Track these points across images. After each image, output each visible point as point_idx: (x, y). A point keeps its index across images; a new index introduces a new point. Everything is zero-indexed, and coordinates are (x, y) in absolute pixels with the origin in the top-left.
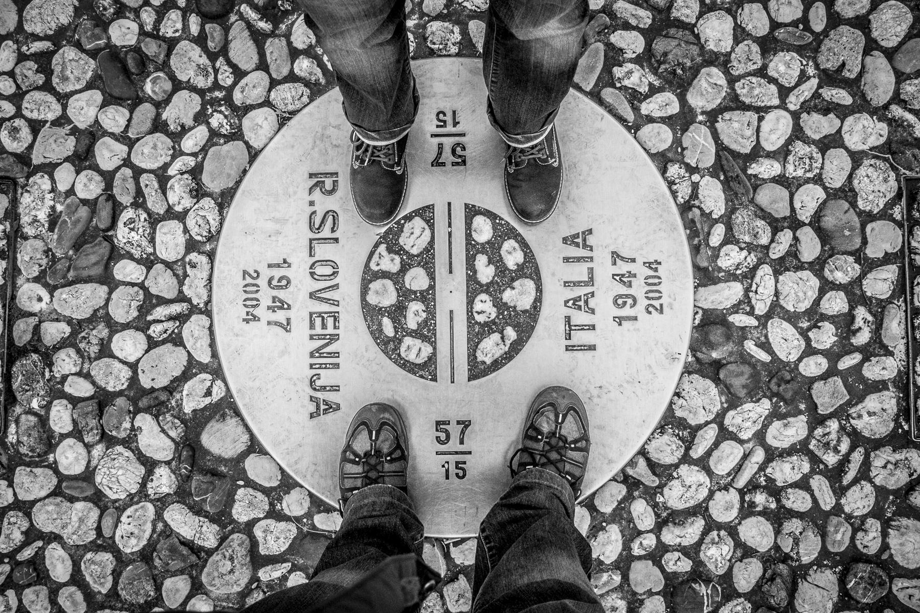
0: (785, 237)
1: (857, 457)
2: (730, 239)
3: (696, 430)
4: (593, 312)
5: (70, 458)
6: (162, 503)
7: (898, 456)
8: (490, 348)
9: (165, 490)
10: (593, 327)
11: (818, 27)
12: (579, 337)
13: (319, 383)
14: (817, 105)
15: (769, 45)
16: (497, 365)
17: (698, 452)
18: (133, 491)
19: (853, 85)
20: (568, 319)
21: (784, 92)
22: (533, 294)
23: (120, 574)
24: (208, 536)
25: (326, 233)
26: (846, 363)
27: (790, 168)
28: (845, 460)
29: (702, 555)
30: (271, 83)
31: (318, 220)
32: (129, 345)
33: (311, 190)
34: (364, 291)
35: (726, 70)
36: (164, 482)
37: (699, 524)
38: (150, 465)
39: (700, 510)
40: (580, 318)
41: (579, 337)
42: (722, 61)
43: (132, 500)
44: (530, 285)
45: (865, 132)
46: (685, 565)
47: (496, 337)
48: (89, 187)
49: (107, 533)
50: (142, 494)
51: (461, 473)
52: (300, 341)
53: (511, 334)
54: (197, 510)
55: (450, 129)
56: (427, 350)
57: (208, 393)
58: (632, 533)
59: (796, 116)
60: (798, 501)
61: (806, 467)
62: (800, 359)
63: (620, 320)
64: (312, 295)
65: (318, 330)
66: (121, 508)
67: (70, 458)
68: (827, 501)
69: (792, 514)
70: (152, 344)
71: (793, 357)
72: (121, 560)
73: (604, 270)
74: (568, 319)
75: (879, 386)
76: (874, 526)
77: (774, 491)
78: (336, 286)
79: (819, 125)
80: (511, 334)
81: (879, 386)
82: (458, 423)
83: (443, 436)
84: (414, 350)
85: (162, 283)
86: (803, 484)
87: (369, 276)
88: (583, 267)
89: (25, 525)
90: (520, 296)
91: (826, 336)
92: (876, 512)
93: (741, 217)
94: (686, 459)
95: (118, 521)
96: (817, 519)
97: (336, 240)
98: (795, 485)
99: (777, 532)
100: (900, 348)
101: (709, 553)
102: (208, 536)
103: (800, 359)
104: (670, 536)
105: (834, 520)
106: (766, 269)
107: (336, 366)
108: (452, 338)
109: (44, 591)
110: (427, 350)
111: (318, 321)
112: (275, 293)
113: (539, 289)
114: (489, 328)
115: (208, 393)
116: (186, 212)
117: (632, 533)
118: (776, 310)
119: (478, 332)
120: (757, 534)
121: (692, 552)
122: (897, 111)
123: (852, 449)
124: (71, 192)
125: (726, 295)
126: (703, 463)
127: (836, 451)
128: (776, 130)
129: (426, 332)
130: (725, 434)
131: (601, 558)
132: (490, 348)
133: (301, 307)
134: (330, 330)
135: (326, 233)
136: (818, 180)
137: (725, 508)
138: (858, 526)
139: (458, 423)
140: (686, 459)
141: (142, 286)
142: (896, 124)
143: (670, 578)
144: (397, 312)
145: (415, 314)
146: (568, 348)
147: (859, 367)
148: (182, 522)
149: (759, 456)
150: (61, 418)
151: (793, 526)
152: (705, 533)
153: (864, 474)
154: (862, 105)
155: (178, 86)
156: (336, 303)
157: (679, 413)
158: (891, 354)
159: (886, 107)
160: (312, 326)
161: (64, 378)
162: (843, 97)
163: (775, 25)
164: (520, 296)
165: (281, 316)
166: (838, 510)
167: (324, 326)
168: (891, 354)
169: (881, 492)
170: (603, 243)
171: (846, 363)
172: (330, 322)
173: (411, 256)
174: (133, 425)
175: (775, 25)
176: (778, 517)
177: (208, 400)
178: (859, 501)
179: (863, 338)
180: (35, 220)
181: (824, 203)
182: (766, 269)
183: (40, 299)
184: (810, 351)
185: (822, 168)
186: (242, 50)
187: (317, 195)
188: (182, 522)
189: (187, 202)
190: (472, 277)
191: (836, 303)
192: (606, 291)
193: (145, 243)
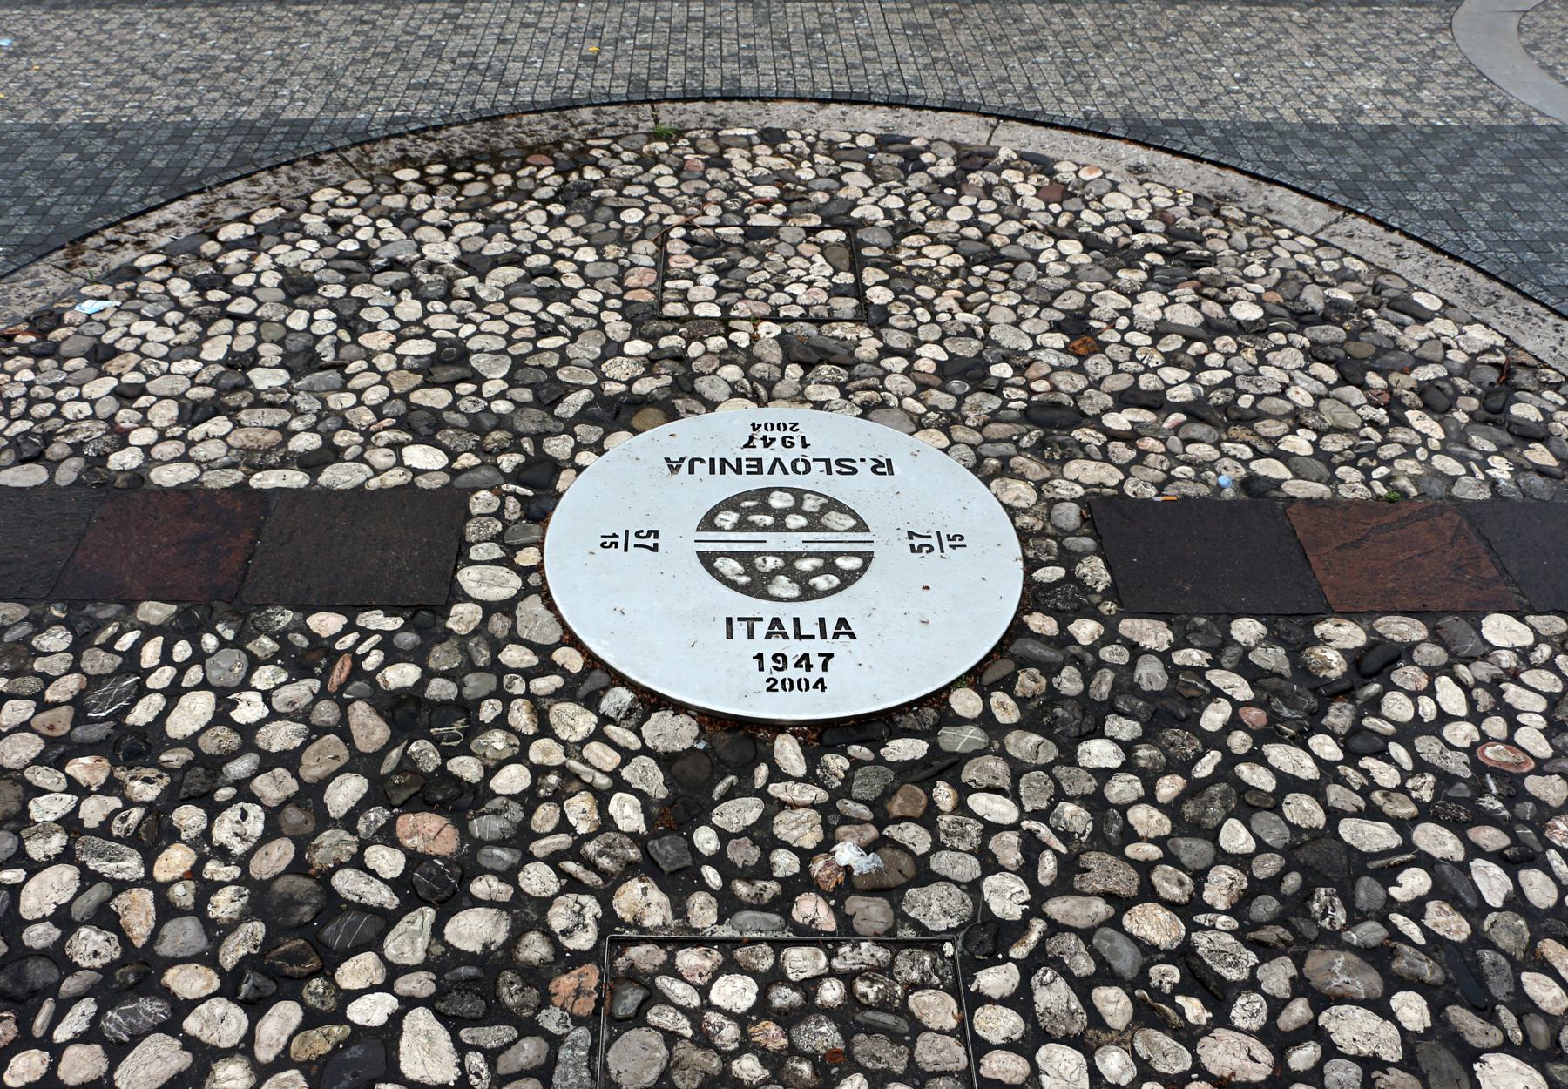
1: (589, 878)
2: (856, 763)
7: (589, 920)
8: (729, 567)
11: (1130, 850)
12: (740, 629)
14: (1032, 847)
15: (1096, 803)
17: (610, 729)
19: (1064, 885)
21: (1041, 816)
22: (784, 594)
26: (712, 876)
27: (948, 818)
28: (590, 865)
35: (1057, 762)
37: (530, 730)
41: (740, 629)
42: (1068, 756)
44: (795, 593)
45: (1006, 897)
47: (740, 569)
55: (946, 544)
59: (1015, 827)
60: (545, 817)
61: (582, 829)
62: (714, 827)
63: (760, 657)
64: (777, 460)
68: (539, 847)
69: (529, 812)
71: (716, 820)
73: (814, 648)
75: (680, 910)
76: (504, 892)
77: (558, 797)
79: (1008, 848)
81: (680, 910)
86: (564, 826)
88: (816, 631)
90: (784, 586)
91: (744, 853)
92: (520, 895)
94: (605, 720)
96: (521, 838)
98: (563, 815)
99: (510, 797)
100: (725, 932)
103: (714, 827)
105: (519, 854)
106: (823, 796)
108: (744, 542)
113: (789, 600)
118: (775, 806)
119: (746, 559)
120: (512, 779)
121: (501, 722)
122: (1038, 926)
123: (603, 873)
126: (598, 735)
127: (600, 854)
128: (999, 809)
130: (627, 755)
132: (729, 567)
135: (835, 468)
136: (937, 846)
137: (544, 752)
138: (509, 876)
140: (605, 720)
142: (1022, 927)
143: (477, 704)
146: (729, 620)
147: (704, 887)
149: (603, 782)
151: (516, 812)
152: (519, 734)
153: (573, 885)
154: (1039, 896)
158: (720, 922)
159: (1043, 916)
162: (1048, 866)
163: (1124, 809)
166: (529, 858)
168: (720, 922)
169: (545, 903)
170: (839, 647)
171: (712, 876)
175: (1124, 809)
176: (529, 800)
178: (538, 879)
179: (742, 888)
181: (912, 853)
182: (823, 796)
184: (724, 836)
185: (953, 849)
190: (800, 555)
191: (785, 863)
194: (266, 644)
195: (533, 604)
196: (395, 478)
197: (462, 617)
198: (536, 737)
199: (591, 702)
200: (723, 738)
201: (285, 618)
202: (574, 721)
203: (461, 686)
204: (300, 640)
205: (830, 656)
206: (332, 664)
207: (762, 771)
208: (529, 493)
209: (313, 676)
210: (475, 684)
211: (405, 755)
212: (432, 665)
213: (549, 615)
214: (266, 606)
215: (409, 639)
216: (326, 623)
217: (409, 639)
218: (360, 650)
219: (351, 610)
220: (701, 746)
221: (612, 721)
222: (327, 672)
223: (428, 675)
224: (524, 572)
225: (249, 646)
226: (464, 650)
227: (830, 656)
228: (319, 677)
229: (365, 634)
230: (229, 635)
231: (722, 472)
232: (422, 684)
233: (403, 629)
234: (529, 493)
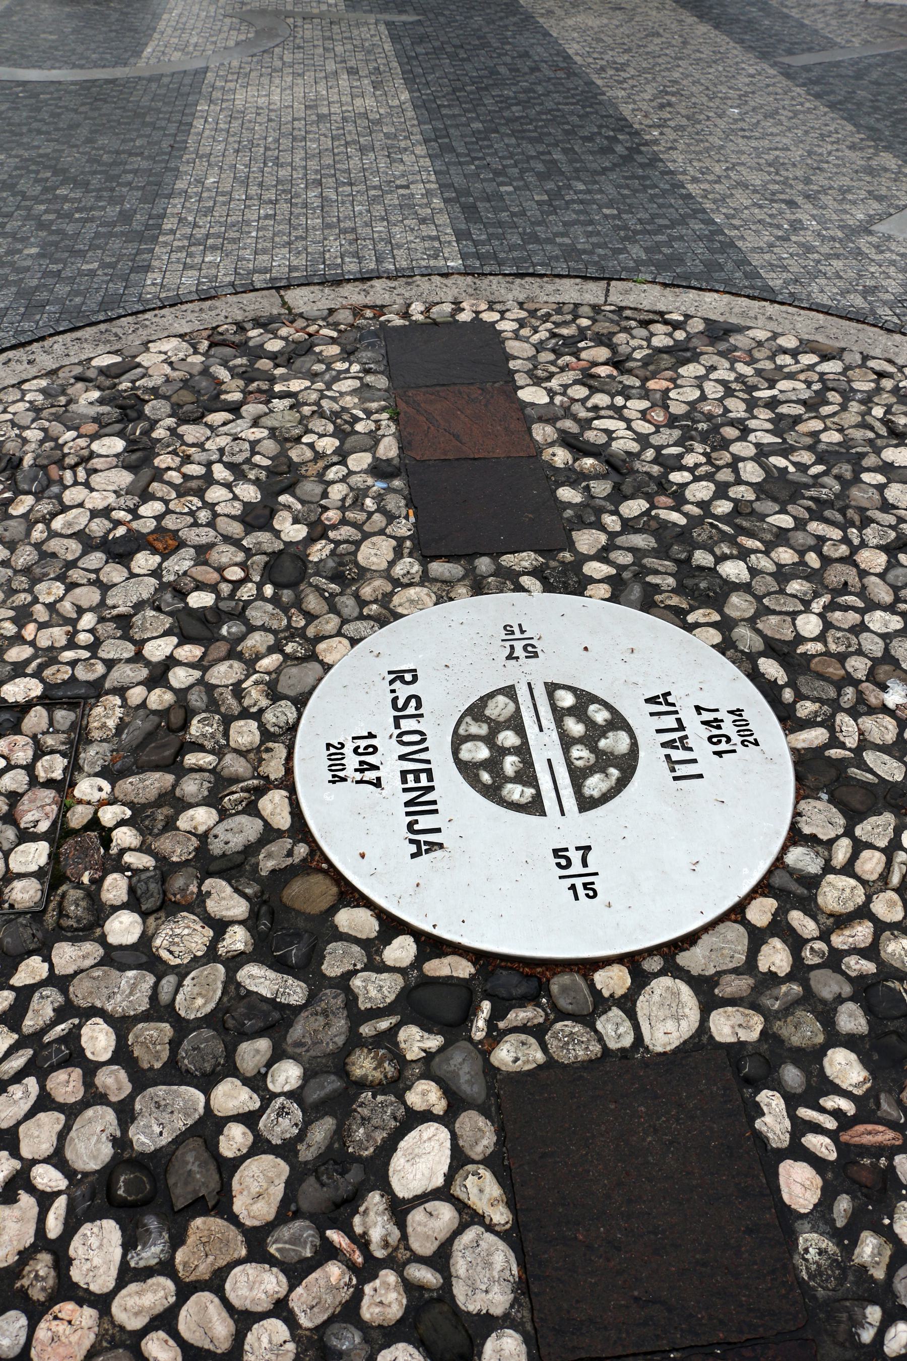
0: (850, 691)
3: (831, 842)
4: (691, 749)
5: (124, 928)
6: (235, 962)
8: (595, 785)
9: (240, 946)
10: (694, 761)
12: (682, 770)
13: (416, 827)
16: (605, 798)
18: (199, 954)
20: (668, 757)
23: (180, 1043)
24: (295, 992)
25: (411, 710)
29: (882, 954)
30: (39, 1204)
31: (400, 703)
32: (201, 817)
33: (391, 682)
34: (456, 752)
36: (237, 939)
38: (220, 927)
39: (863, 913)
40: (678, 755)
43: (196, 962)
46: (869, 967)
48: (159, 699)
49: (164, 996)
50: (211, 955)
51: (591, 893)
52: (394, 794)
53: (614, 772)
54: (280, 965)
56: (530, 792)
57: (290, 853)
58: (796, 943)
59: (821, 615)
65: (411, 784)
66: (182, 972)
67: (124, 928)
70: (224, 815)
72: (182, 1027)
74: (668, 757)
78: (426, 749)
80: (614, 772)
82: (578, 849)
83: (563, 862)
84: (516, 792)
85: (234, 765)
87: (458, 741)
89: (60, 999)
93: (801, 680)
95: (180, 985)
97: (421, 716)
101: (890, 949)
102: (295, 992)
104: (839, 940)
107: (435, 811)
109: (77, 1073)
110: (530, 792)
111: (410, 777)
112: (363, 758)
114: (590, 771)
115: (290, 853)
116: (261, 711)
117: (796, 943)
124: (143, 705)
125: (815, 736)
126: (848, 870)
129: (527, 776)
131: (773, 969)
133: (390, 765)
134: (424, 782)
135: (411, 710)
139: (578, 849)
141: (213, 771)
144: (493, 764)
145: (510, 764)
146: (676, 779)
148: (259, 979)
150: (115, 888)
155: (252, 629)
156: (428, 762)
157: (807, 830)
160: (404, 781)
161: (122, 851)
164: (618, 742)
165: (370, 775)
167: (417, 780)
172: (423, 776)
173: (498, 723)
174: (200, 890)
177: (289, 861)
180: (104, 726)
183: (100, 789)
186: (313, 602)
187: (398, 685)
188: (259, 979)
189: (264, 702)
192: (697, 733)
193: (219, 736)
194: (868, 1248)
195: (695, 960)
196: (483, 1190)
197: (726, 1026)
198: (873, 918)
199: (812, 882)
200: (811, 780)
201: (812, 1244)
202: (838, 893)
203: (840, 999)
204: (843, 1205)
205: (588, 848)
206: (864, 1150)
207: (835, 753)
208: (486, 1006)
209: (891, 1168)
210: (828, 986)
211: (393, 1031)
212: (820, 1039)
213: (706, 940)
214: (801, 1283)
215: (792, 1075)
216: (799, 1185)
217: (792, 1075)
218: (830, 1123)
219: (770, 1159)
220: (825, 797)
221: (828, 861)
222: (879, 1150)
223: (835, 1039)
224: (641, 979)
225: (879, 1274)
226: (787, 1010)
227: (588, 848)
228: (891, 1159)
229: (800, 1128)
230: (874, 1313)
231: (408, 814)
232: (851, 1042)
233: (777, 1086)
234: (486, 1006)
